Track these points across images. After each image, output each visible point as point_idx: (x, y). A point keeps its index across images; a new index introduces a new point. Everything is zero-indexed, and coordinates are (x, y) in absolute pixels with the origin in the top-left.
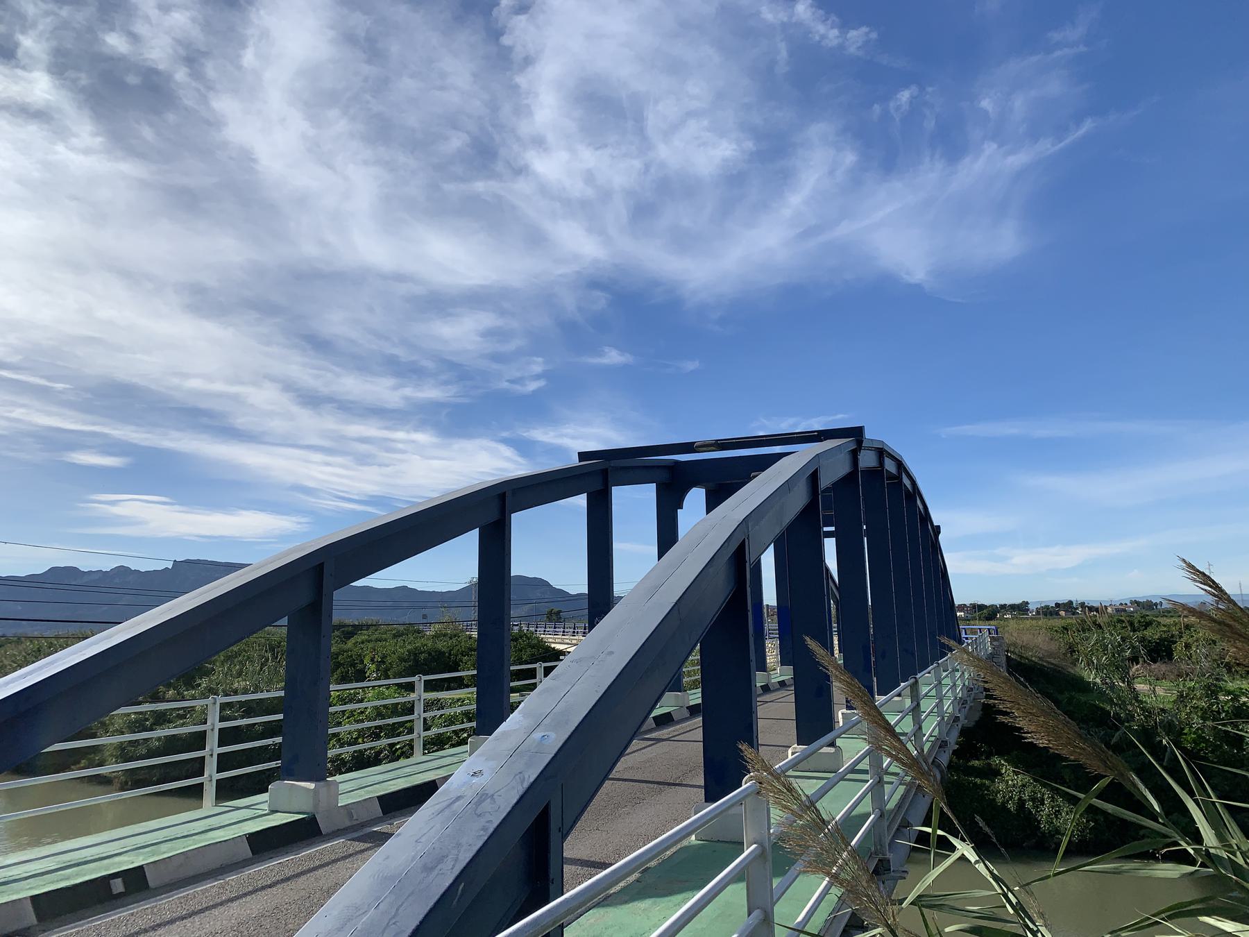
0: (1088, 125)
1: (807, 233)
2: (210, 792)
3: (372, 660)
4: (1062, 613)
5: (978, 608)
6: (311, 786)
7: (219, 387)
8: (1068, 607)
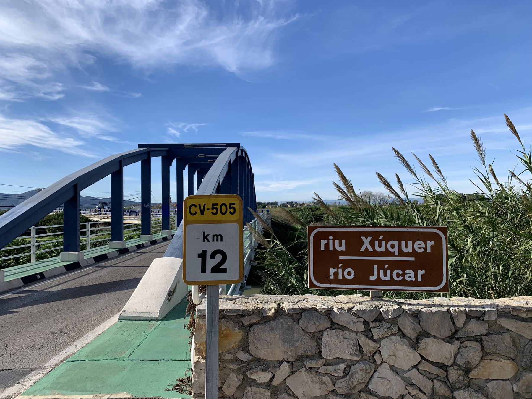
0: (297, 16)
1: (187, 43)
4: (289, 206)
5: (261, 204)
6: (77, 253)
8: (291, 204)
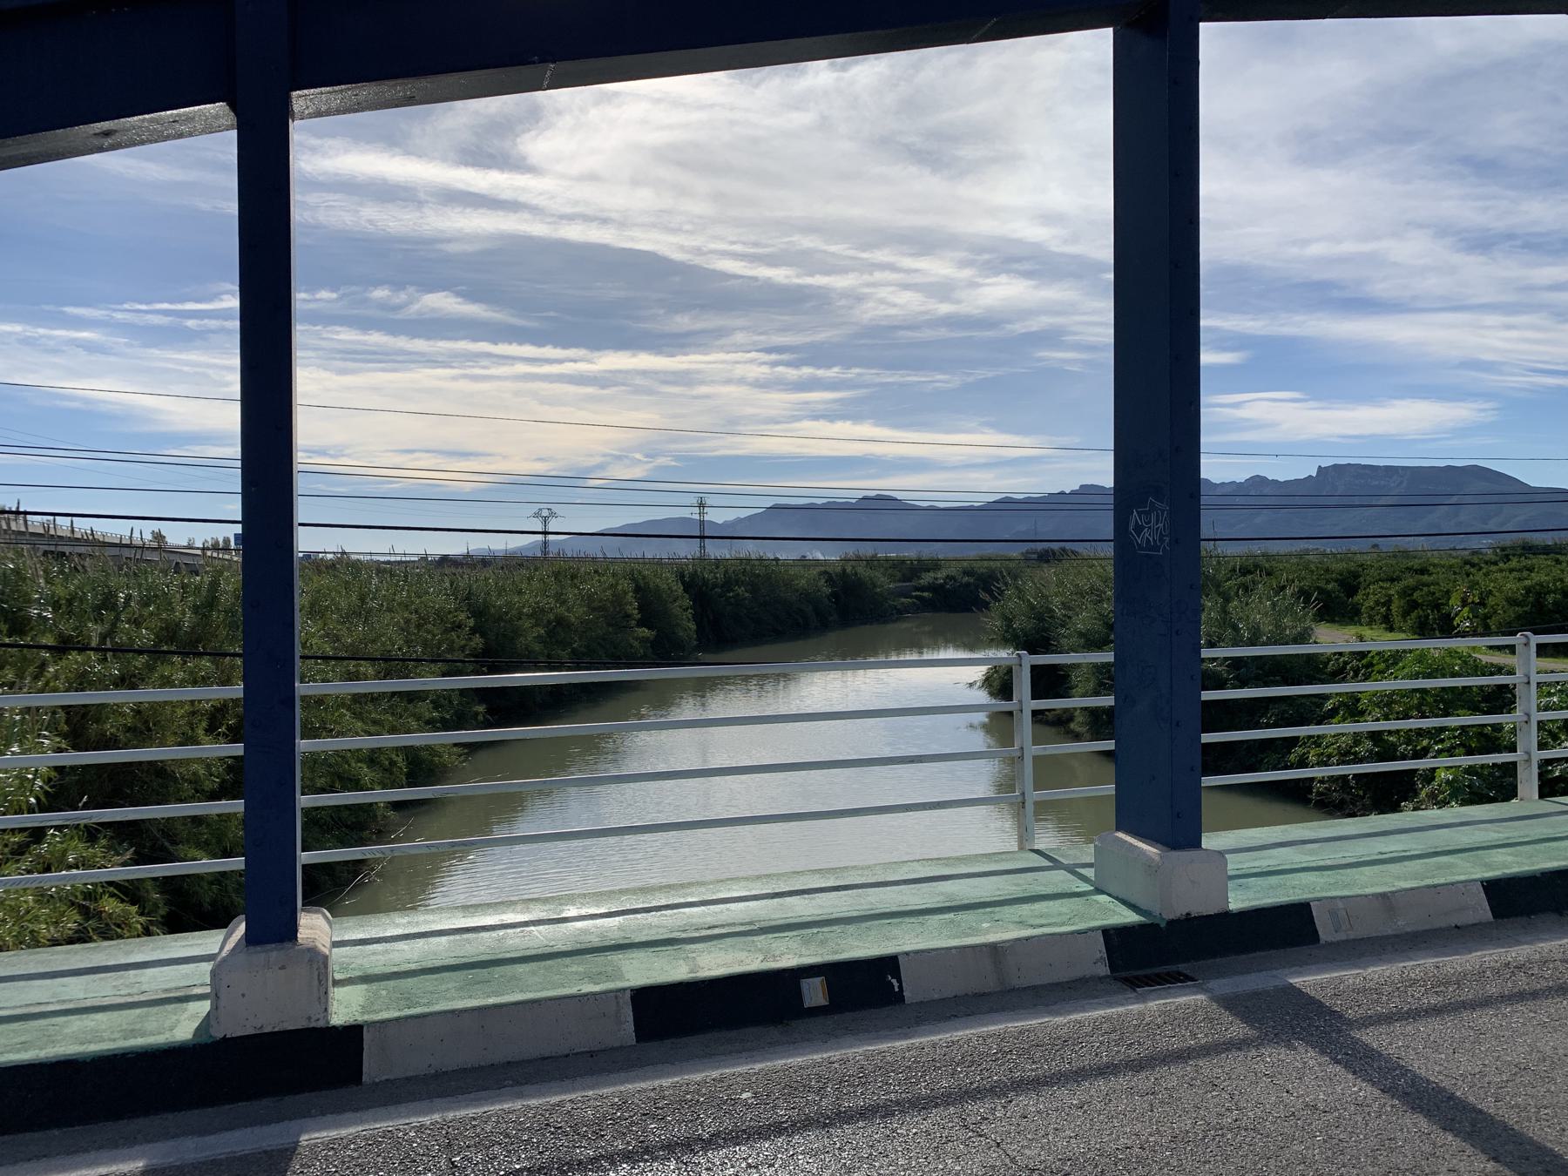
2: (1528, 783)
3: (1464, 603)
7: (1349, 247)
